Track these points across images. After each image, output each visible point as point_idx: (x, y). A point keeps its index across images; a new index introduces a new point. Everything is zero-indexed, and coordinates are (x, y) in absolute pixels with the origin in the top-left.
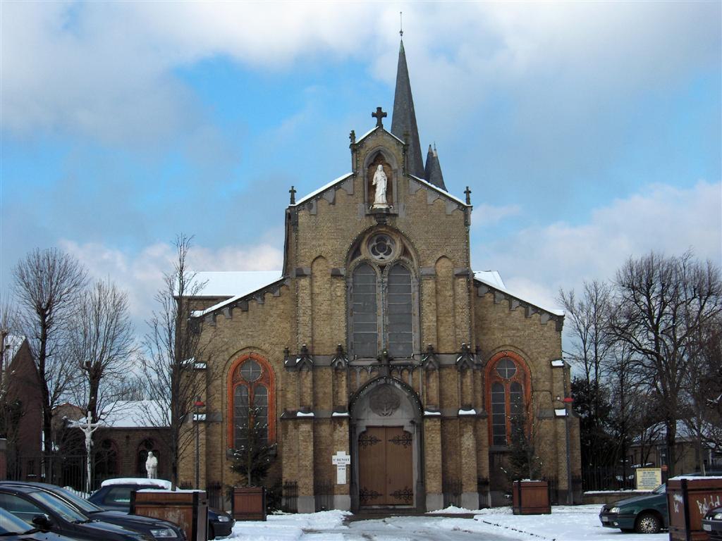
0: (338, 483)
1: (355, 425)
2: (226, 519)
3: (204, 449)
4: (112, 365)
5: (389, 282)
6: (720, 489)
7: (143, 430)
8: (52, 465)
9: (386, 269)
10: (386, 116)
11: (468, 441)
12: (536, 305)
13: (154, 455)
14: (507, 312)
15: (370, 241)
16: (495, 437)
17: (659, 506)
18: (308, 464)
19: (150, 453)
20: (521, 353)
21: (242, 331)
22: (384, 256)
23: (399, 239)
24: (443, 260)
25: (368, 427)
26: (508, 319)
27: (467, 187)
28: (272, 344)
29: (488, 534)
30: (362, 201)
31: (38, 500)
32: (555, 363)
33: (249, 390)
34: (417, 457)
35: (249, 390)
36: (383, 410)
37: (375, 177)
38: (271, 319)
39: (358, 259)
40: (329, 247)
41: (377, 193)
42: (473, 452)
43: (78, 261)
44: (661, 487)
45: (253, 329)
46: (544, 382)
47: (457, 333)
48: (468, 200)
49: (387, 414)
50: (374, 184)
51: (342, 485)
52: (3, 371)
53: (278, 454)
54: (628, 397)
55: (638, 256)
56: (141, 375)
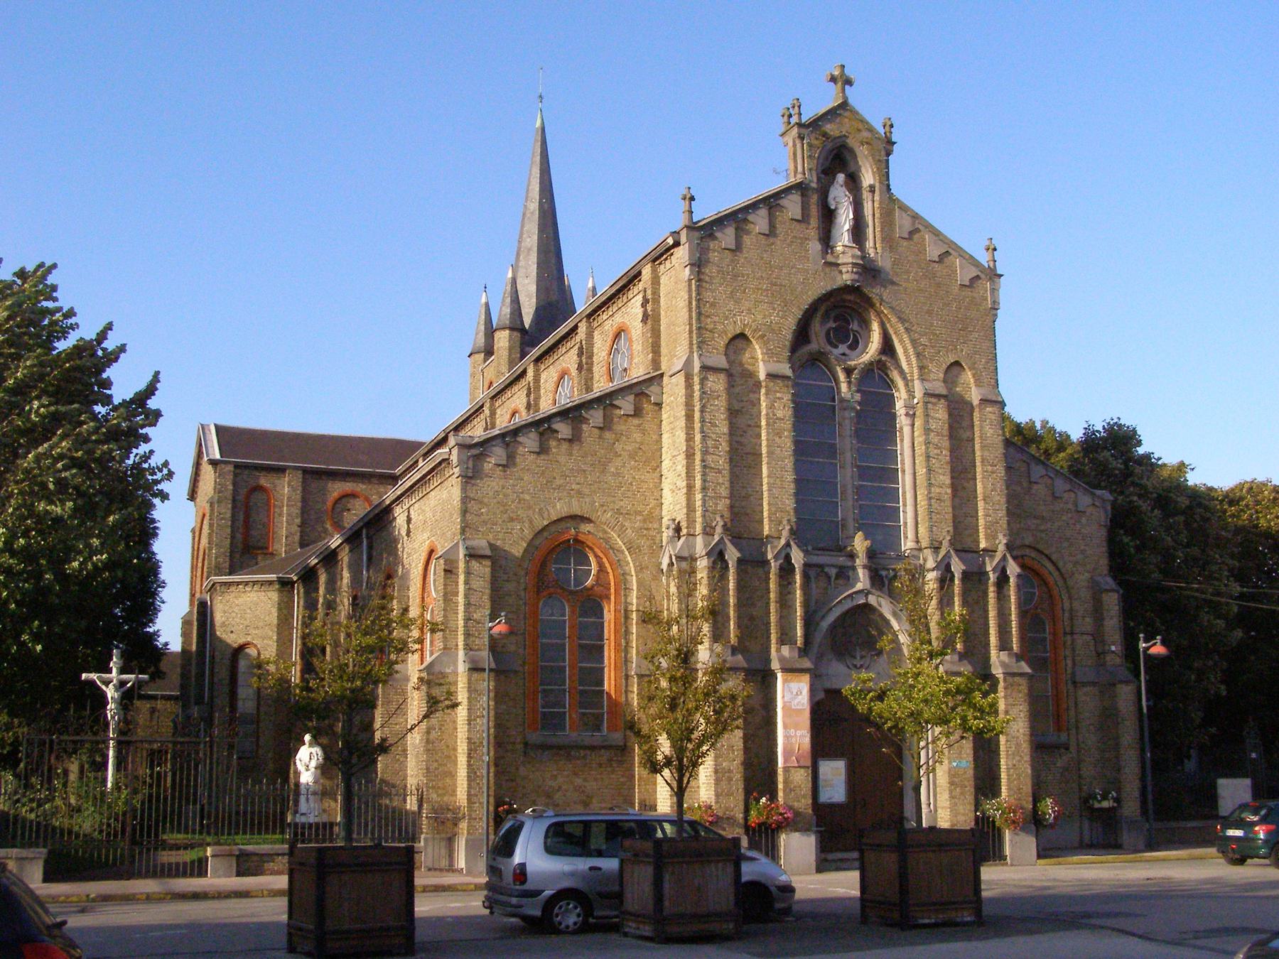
0: (1221, 782)
1: (851, 550)
2: (667, 826)
8: (702, 411)
9: (855, 375)
12: (547, 141)
13: (316, 741)
14: (1025, 484)
15: (826, 317)
16: (836, 459)
17: (430, 656)
19: (307, 738)
20: (1048, 565)
21: (559, 482)
22: (848, 352)
24: (1025, 464)
26: (1027, 497)
27: (54, 266)
28: (619, 512)
32: (137, 516)
36: (855, 657)
38: (618, 462)
39: (805, 350)
40: (759, 317)
42: (1024, 745)
43: (783, 135)
44: (338, 690)
45: (580, 479)
46: (1084, 617)
48: (660, 255)
49: (862, 666)
51: (1245, 833)
52: (112, 739)
53: (628, 744)
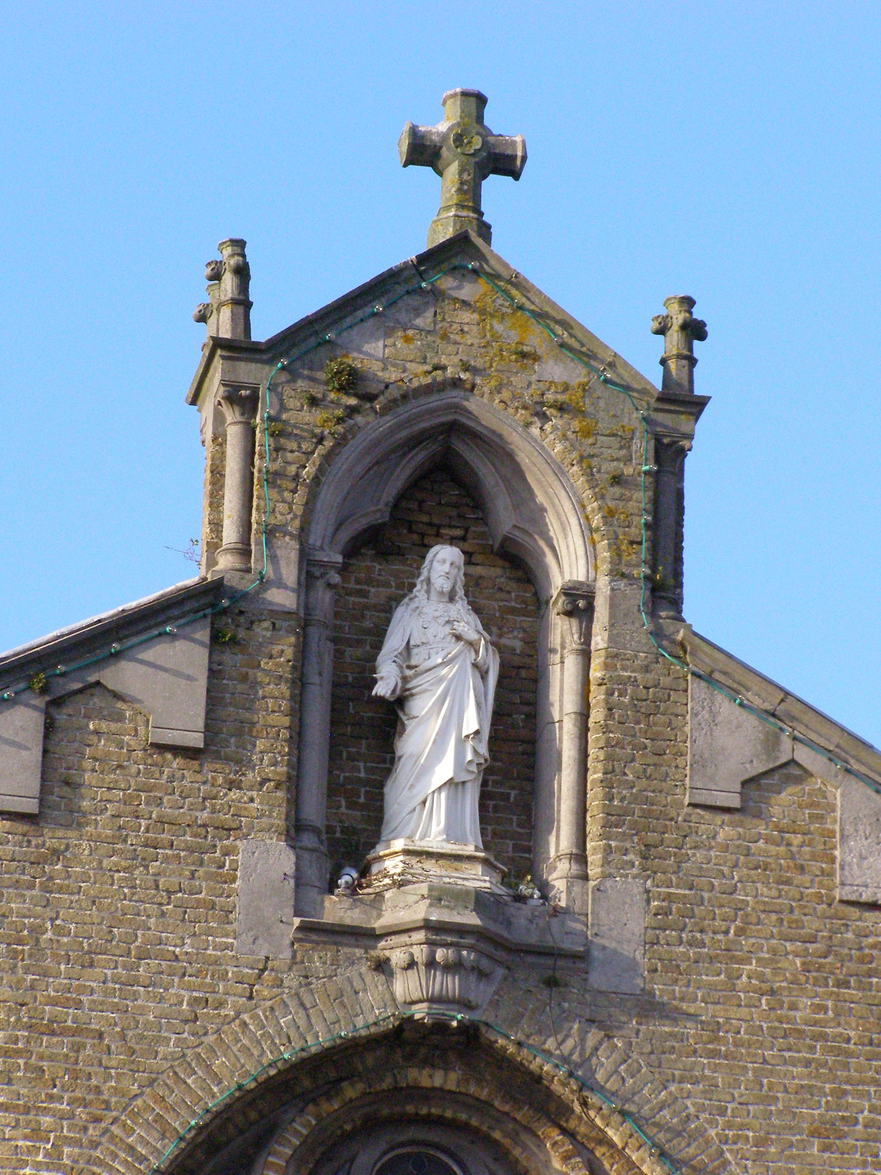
3: (626, 953)
4: (628, 400)
5: (53, 977)
6: (873, 906)
7: (357, 296)
10: (516, 175)
11: (493, 483)
18: (378, 567)
23: (61, 681)
25: (98, 683)
29: (326, 754)
30: (278, 818)
31: (171, 593)
33: (306, 427)
34: (572, 762)
35: (306, 427)
37: (393, 642)
41: (404, 772)
47: (502, 992)
50: (382, 689)
54: (390, 882)
55: (707, 323)
56: (303, 844)
